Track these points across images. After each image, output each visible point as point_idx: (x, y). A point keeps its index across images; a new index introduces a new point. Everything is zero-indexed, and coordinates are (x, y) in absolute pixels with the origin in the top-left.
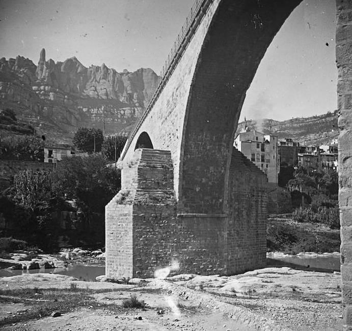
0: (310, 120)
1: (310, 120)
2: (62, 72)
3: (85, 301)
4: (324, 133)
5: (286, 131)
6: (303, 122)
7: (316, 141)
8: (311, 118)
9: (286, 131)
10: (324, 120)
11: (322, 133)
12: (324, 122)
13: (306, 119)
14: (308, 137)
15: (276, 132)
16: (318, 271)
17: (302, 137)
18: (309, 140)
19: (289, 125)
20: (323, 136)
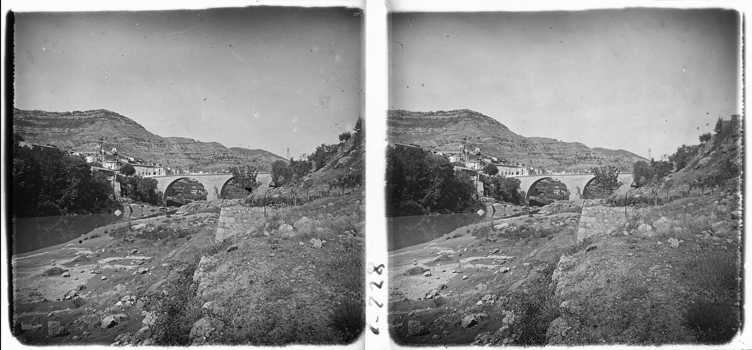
0: (52, 115)
1: (52, 115)
2: (353, 14)
3: (174, 287)
4: (430, 129)
5: (31, 121)
6: (45, 115)
7: (59, 134)
8: (416, 113)
9: (31, 121)
10: (428, 117)
11: (429, 128)
12: (428, 119)
13: (49, 113)
14: (416, 129)
15: (21, 119)
16: (108, 257)
17: (47, 129)
18: (54, 133)
19: (396, 115)
20: (429, 131)
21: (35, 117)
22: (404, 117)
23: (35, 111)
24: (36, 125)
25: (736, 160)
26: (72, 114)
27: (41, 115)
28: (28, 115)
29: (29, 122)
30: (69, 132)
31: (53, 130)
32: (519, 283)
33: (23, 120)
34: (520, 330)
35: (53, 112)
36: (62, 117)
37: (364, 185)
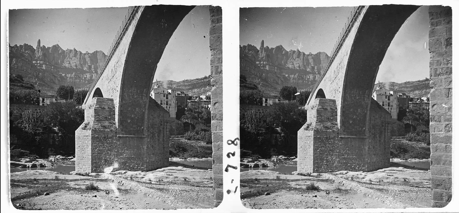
1: (194, 81)
5: (180, 87)
6: (190, 82)
7: (198, 93)
9: (180, 87)
17: (412, 92)
21: (183, 84)
22: (372, 183)
23: (183, 81)
24: (406, 91)
25: (173, 160)
26: (208, 78)
27: (187, 83)
28: (401, 86)
29: (180, 88)
30: (425, 92)
31: (193, 91)
32: (435, 108)
33: (398, 89)
34: (426, 108)
35: (417, 80)
36: (422, 83)
37: (451, 99)
